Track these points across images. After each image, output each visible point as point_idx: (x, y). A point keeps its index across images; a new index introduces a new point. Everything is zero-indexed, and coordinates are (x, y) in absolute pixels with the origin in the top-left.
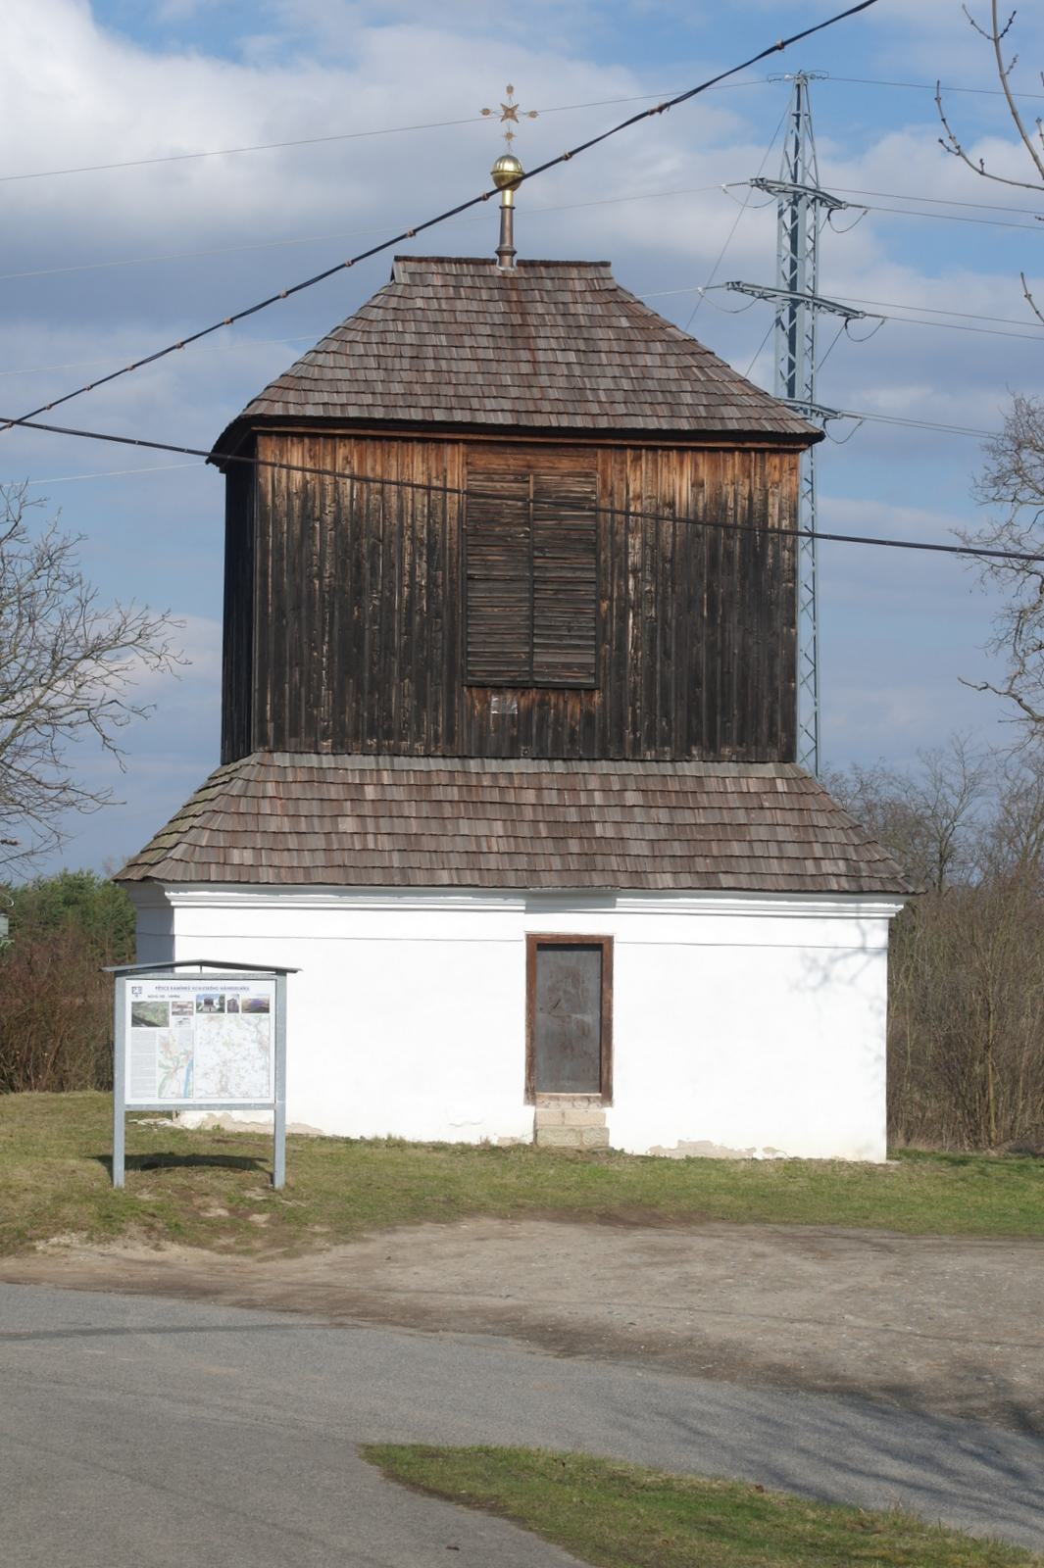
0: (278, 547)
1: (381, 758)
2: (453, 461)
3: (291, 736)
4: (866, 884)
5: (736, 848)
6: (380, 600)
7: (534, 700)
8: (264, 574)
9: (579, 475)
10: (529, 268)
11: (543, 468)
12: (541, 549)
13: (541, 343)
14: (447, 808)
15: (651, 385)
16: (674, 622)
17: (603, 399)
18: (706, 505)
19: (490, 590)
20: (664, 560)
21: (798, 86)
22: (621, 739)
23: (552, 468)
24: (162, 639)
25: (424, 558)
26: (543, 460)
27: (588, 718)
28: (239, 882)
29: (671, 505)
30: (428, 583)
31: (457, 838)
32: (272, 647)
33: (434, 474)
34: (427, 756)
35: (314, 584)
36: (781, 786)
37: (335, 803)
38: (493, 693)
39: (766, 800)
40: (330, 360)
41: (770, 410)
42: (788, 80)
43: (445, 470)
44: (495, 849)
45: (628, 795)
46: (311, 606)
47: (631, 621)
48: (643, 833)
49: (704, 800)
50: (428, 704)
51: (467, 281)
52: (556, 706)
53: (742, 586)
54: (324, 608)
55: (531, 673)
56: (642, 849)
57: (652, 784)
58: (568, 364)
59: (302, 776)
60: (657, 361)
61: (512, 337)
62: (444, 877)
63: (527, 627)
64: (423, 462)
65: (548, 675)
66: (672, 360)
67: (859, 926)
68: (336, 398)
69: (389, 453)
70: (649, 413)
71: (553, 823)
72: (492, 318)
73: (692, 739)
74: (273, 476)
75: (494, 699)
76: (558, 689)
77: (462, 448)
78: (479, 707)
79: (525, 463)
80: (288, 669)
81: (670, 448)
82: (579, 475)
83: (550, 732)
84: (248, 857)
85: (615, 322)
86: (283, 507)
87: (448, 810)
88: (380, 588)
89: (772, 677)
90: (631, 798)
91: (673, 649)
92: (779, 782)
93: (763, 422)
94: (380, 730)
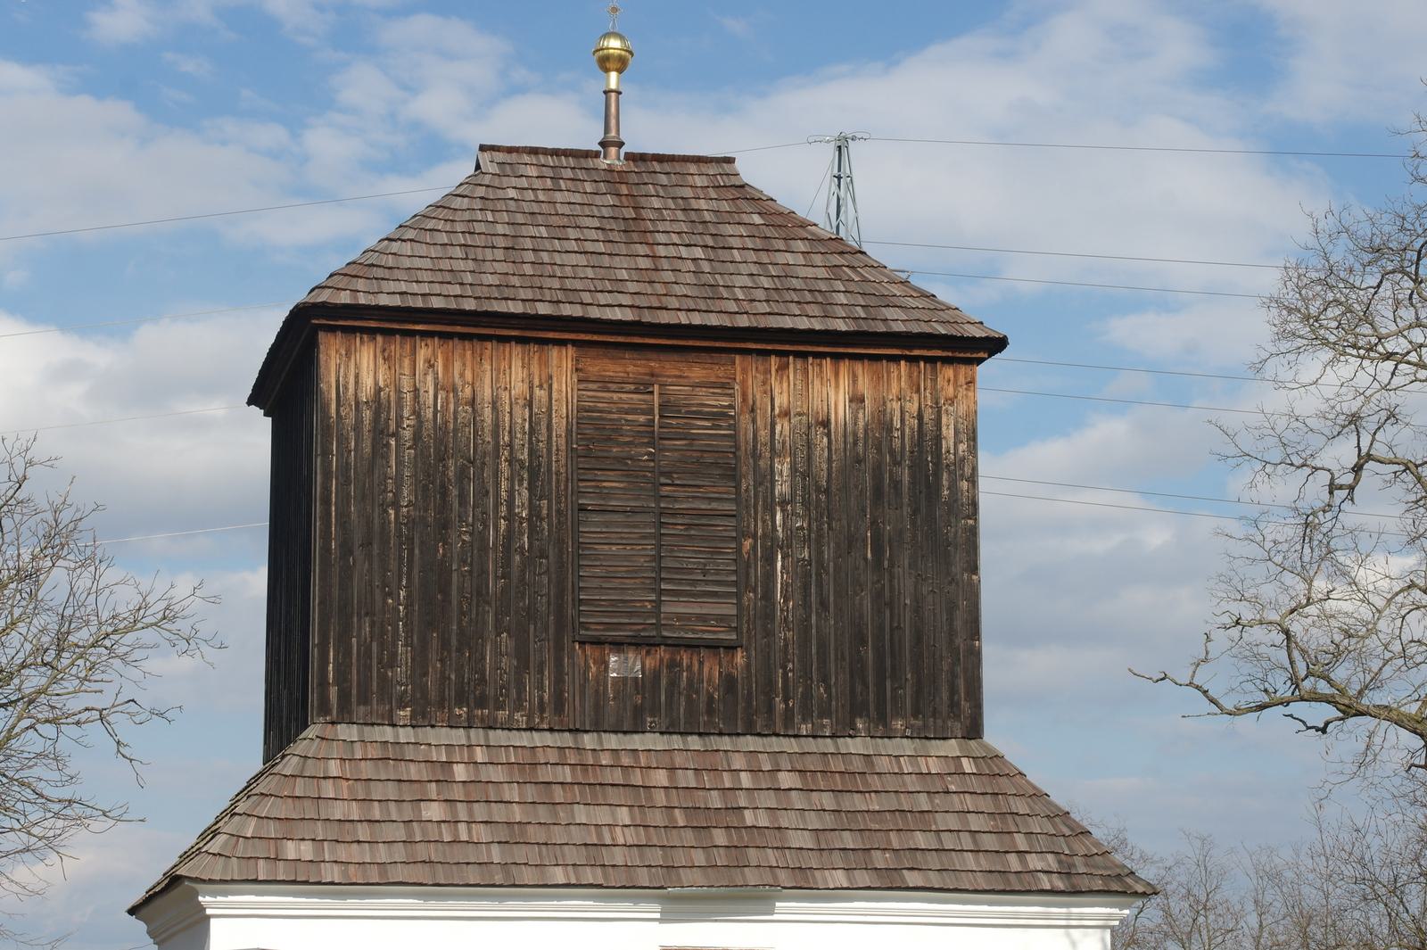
0: (344, 468)
1: (472, 731)
2: (560, 367)
3: (359, 704)
4: (1084, 883)
5: (921, 840)
6: (471, 534)
7: (661, 660)
8: (326, 502)
9: (713, 385)
10: (640, 163)
11: (669, 377)
12: (668, 474)
13: (661, 238)
14: (558, 790)
15: (796, 283)
16: (831, 564)
17: (741, 297)
18: (867, 425)
19: (607, 524)
20: (818, 490)
21: (840, 147)
22: (770, 709)
23: (680, 377)
24: (190, 621)
25: (525, 484)
26: (670, 368)
27: (729, 683)
28: (294, 882)
29: (826, 424)
30: (530, 514)
31: (572, 827)
32: (336, 592)
33: (536, 382)
34: (531, 729)
35: (389, 515)
36: (968, 766)
37: (416, 786)
38: (610, 650)
39: (952, 783)
40: (407, 248)
41: (941, 313)
42: (828, 142)
43: (551, 377)
44: (621, 841)
45: (781, 775)
46: (385, 541)
47: (779, 564)
48: (805, 821)
49: (875, 782)
50: (531, 665)
51: (568, 173)
52: (690, 667)
53: (913, 523)
54: (401, 544)
55: (658, 626)
56: (806, 840)
57: (812, 764)
58: (694, 260)
59: (374, 752)
60: (801, 259)
61: (625, 231)
62: (559, 875)
63: (653, 569)
64: (523, 367)
65: (681, 628)
66: (818, 259)
67: (1068, 935)
68: (415, 288)
69: (481, 355)
70: (798, 312)
71: (690, 810)
72: (599, 211)
73: (857, 709)
74: (338, 381)
75: (613, 659)
76: (692, 646)
77: (571, 350)
78: (594, 669)
79: (647, 370)
80: (355, 619)
81: (822, 355)
82: (713, 385)
83: (683, 699)
84: (307, 851)
85: (745, 218)
86: (350, 420)
87: (559, 794)
88: (470, 519)
89: (952, 633)
90: (786, 780)
91: (832, 599)
92: (965, 761)
93: (934, 324)
94: (472, 696)
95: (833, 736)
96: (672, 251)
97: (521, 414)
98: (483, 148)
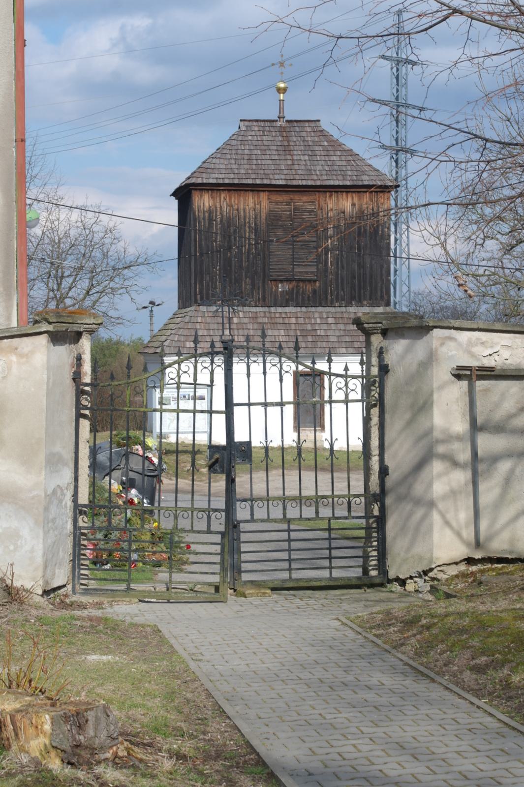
8: (195, 241)
15: (336, 168)
26: (296, 197)
27: (314, 291)
29: (344, 213)
32: (199, 267)
40: (218, 161)
45: (329, 319)
51: (267, 129)
52: (303, 287)
55: (293, 275)
57: (338, 315)
59: (210, 314)
60: (338, 158)
68: (220, 176)
73: (352, 298)
77: (267, 193)
81: (343, 192)
85: (322, 143)
86: (202, 216)
89: (382, 275)
90: (330, 320)
95: (345, 306)
96: (298, 157)
97: (252, 213)
98: (241, 120)
